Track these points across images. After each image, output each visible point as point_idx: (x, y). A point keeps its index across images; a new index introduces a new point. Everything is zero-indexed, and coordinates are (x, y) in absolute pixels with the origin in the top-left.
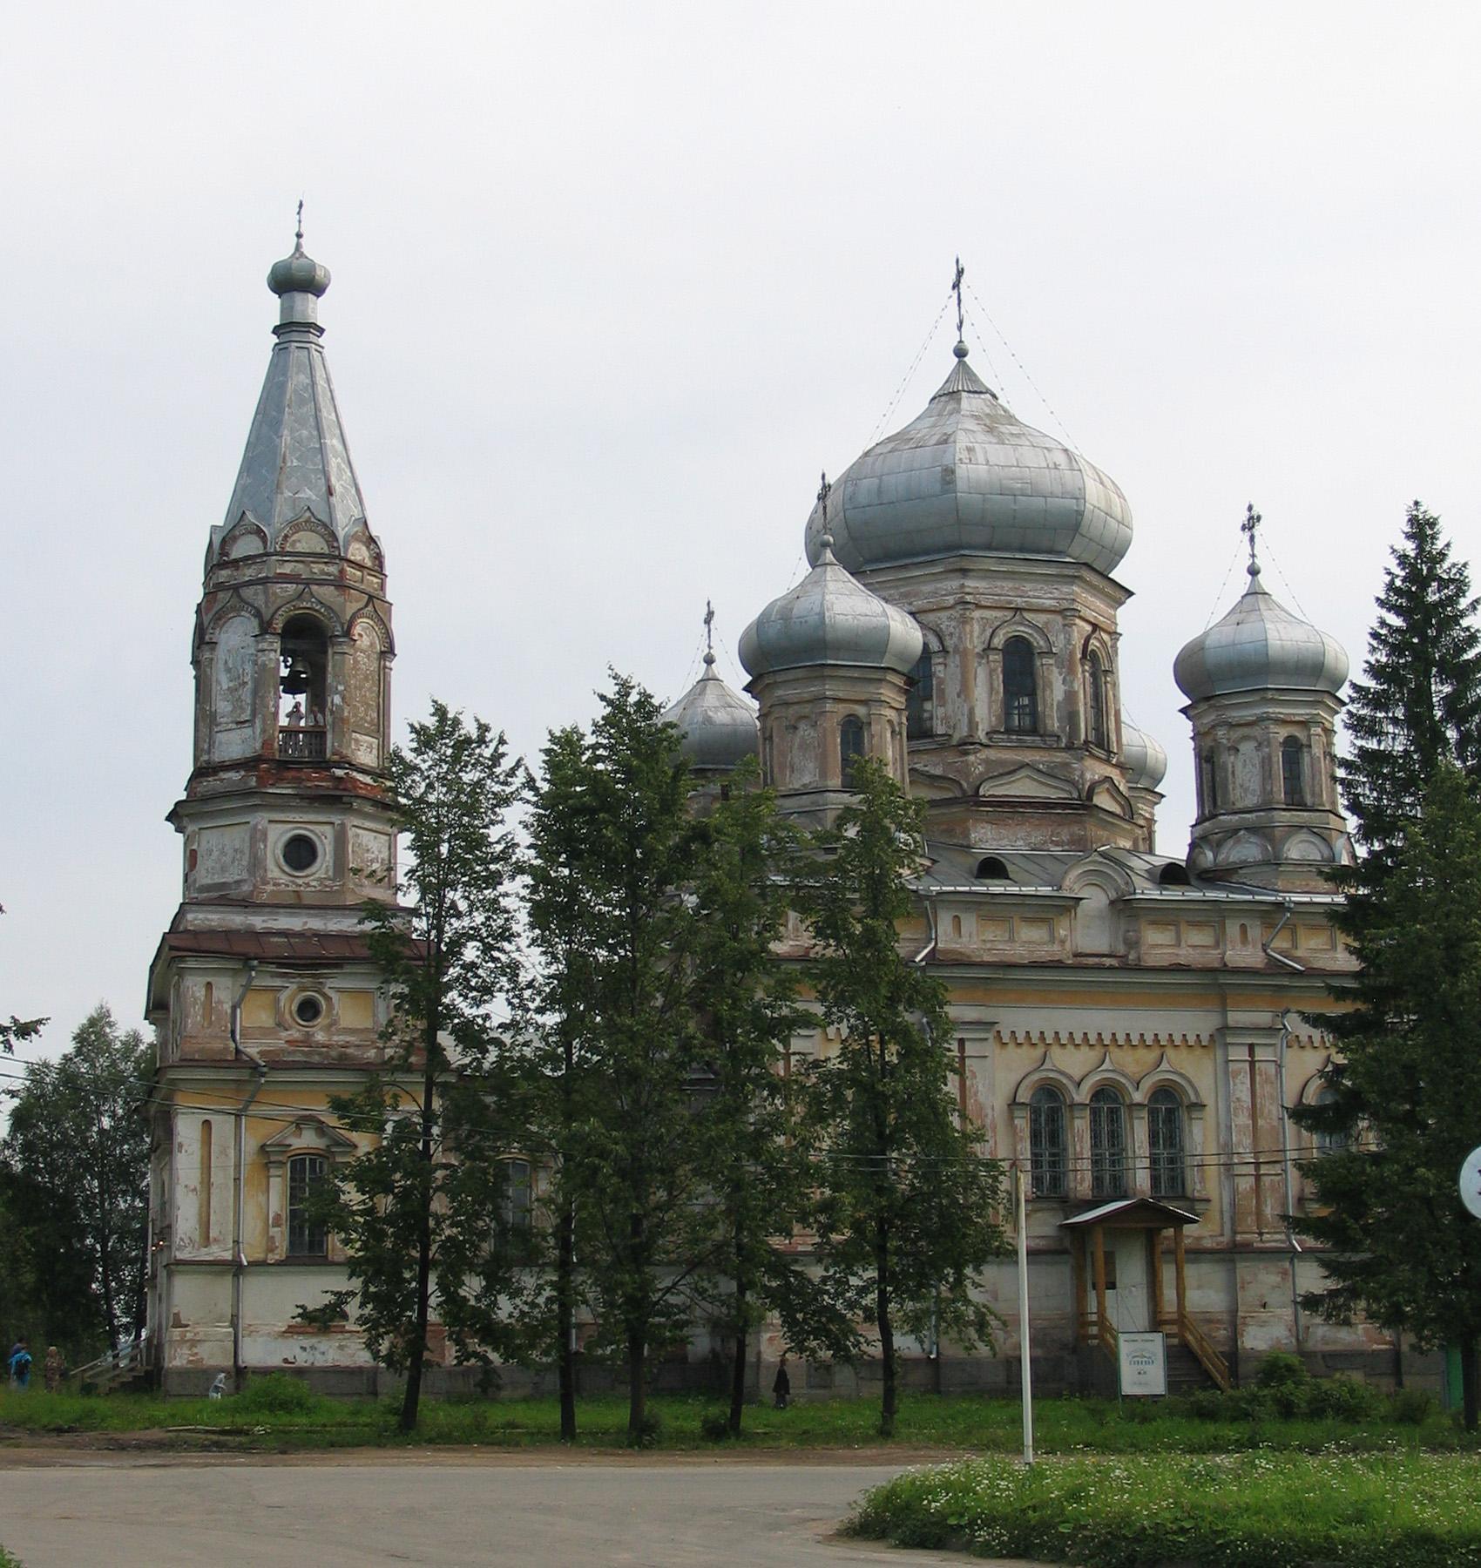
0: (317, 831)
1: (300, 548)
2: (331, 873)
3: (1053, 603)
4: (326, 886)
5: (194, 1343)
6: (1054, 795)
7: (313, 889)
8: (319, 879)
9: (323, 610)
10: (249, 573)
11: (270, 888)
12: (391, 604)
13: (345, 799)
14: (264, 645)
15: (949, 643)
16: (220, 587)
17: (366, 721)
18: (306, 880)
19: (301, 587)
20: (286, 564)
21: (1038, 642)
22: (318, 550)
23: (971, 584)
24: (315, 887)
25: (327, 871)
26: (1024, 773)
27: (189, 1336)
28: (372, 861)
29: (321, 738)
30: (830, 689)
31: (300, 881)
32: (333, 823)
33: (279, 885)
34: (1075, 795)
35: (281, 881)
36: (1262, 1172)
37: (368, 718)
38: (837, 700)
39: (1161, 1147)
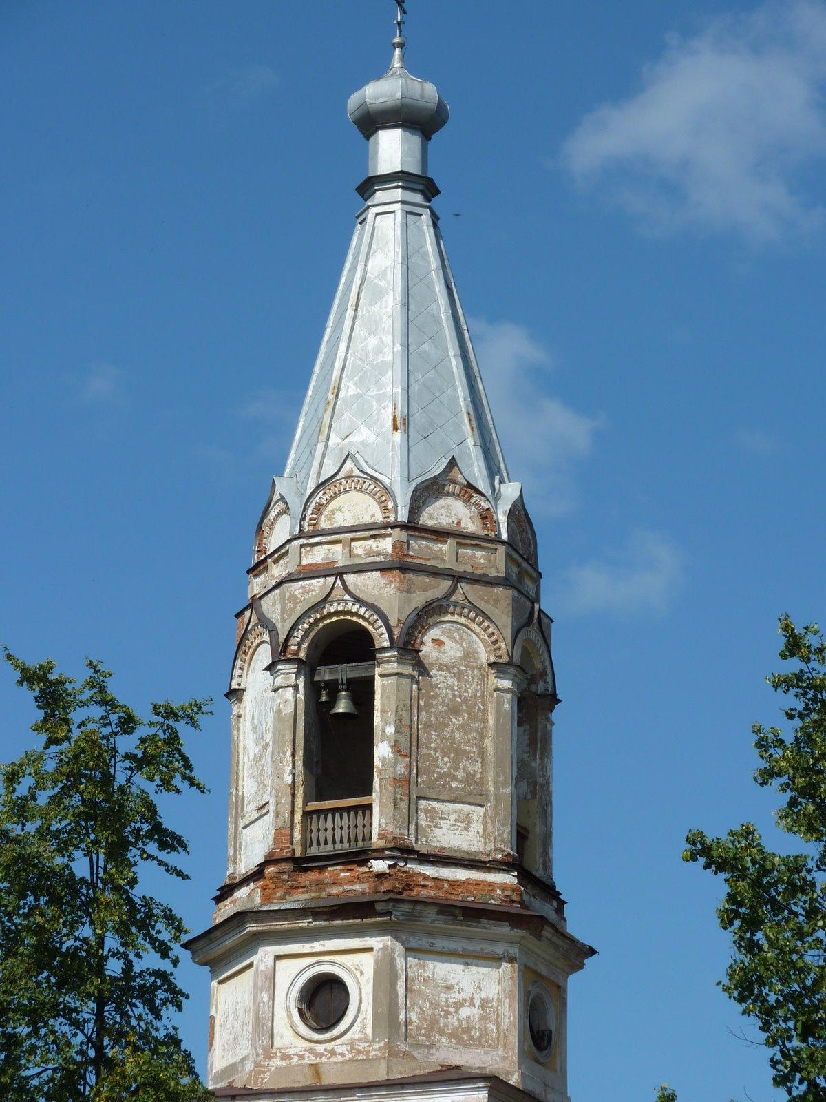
0: (349, 964)
1: (341, 521)
2: (369, 1031)
4: (359, 1052)
7: (340, 1059)
8: (352, 1044)
9: (362, 611)
11: (276, 1063)
12: (552, 621)
13: (379, 907)
14: (279, 681)
17: (455, 778)
18: (329, 1046)
19: (331, 580)
20: (316, 548)
22: (367, 519)
24: (342, 1055)
25: (363, 1027)
28: (459, 1005)
29: (368, 812)
31: (320, 1048)
32: (370, 949)
33: (289, 1057)
35: (293, 1051)
36: (297, 647)
37: (460, 774)
39: (314, 806)
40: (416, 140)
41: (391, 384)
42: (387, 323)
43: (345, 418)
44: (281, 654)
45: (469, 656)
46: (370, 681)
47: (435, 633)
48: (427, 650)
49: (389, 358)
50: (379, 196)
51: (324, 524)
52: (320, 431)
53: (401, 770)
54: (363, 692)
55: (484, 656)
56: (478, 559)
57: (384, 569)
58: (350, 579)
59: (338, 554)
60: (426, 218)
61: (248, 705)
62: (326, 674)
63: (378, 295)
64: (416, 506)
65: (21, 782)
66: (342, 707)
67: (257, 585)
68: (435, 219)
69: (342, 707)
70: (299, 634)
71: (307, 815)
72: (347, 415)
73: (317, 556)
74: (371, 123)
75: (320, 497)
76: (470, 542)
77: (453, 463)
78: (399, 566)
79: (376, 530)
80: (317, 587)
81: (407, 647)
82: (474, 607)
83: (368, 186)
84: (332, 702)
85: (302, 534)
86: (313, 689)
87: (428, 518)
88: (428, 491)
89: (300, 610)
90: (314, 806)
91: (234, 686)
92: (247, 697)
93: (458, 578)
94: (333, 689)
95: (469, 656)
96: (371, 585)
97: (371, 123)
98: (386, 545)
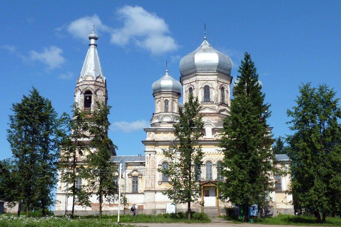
3: (213, 79)
5: (59, 206)
6: (212, 112)
10: (81, 84)
14: (81, 95)
15: (195, 88)
16: (263, 122)
19: (87, 86)
21: (210, 86)
22: (91, 80)
23: (198, 77)
26: (207, 108)
27: (58, 205)
30: (162, 95)
34: (216, 112)
38: (164, 97)
39: (85, 108)
40: (95, 40)
41: (93, 66)
42: (92, 60)
43: (88, 69)
44: (82, 93)
45: (101, 94)
46: (91, 96)
47: (98, 92)
48: (97, 93)
49: (93, 63)
50: (91, 46)
51: (86, 80)
52: (85, 70)
53: (94, 105)
54: (90, 97)
55: (102, 95)
56: (102, 85)
57: (93, 85)
58: (89, 86)
59: (88, 83)
60: (96, 49)
61: (77, 97)
62: (86, 95)
63: (91, 56)
64: (96, 79)
65: (92, 196)
66: (88, 99)
67: (78, 85)
68: (97, 49)
69: (88, 99)
70: (84, 91)
71: (84, 109)
72: (88, 69)
73: (86, 83)
74: (90, 38)
75: (86, 77)
76: (164, 123)
77: (100, 75)
78: (95, 85)
79: (92, 81)
80: (86, 86)
81: (95, 93)
82: (102, 90)
83: (90, 45)
84: (87, 98)
85: (84, 81)
86: (85, 97)
87: (97, 80)
88: (97, 78)
89: (84, 88)
90: (85, 108)
91: (75, 95)
92: (76, 96)
93: (100, 87)
94: (87, 97)
95: (101, 94)
96: (92, 86)
97: (90, 38)
98: (93, 83)
